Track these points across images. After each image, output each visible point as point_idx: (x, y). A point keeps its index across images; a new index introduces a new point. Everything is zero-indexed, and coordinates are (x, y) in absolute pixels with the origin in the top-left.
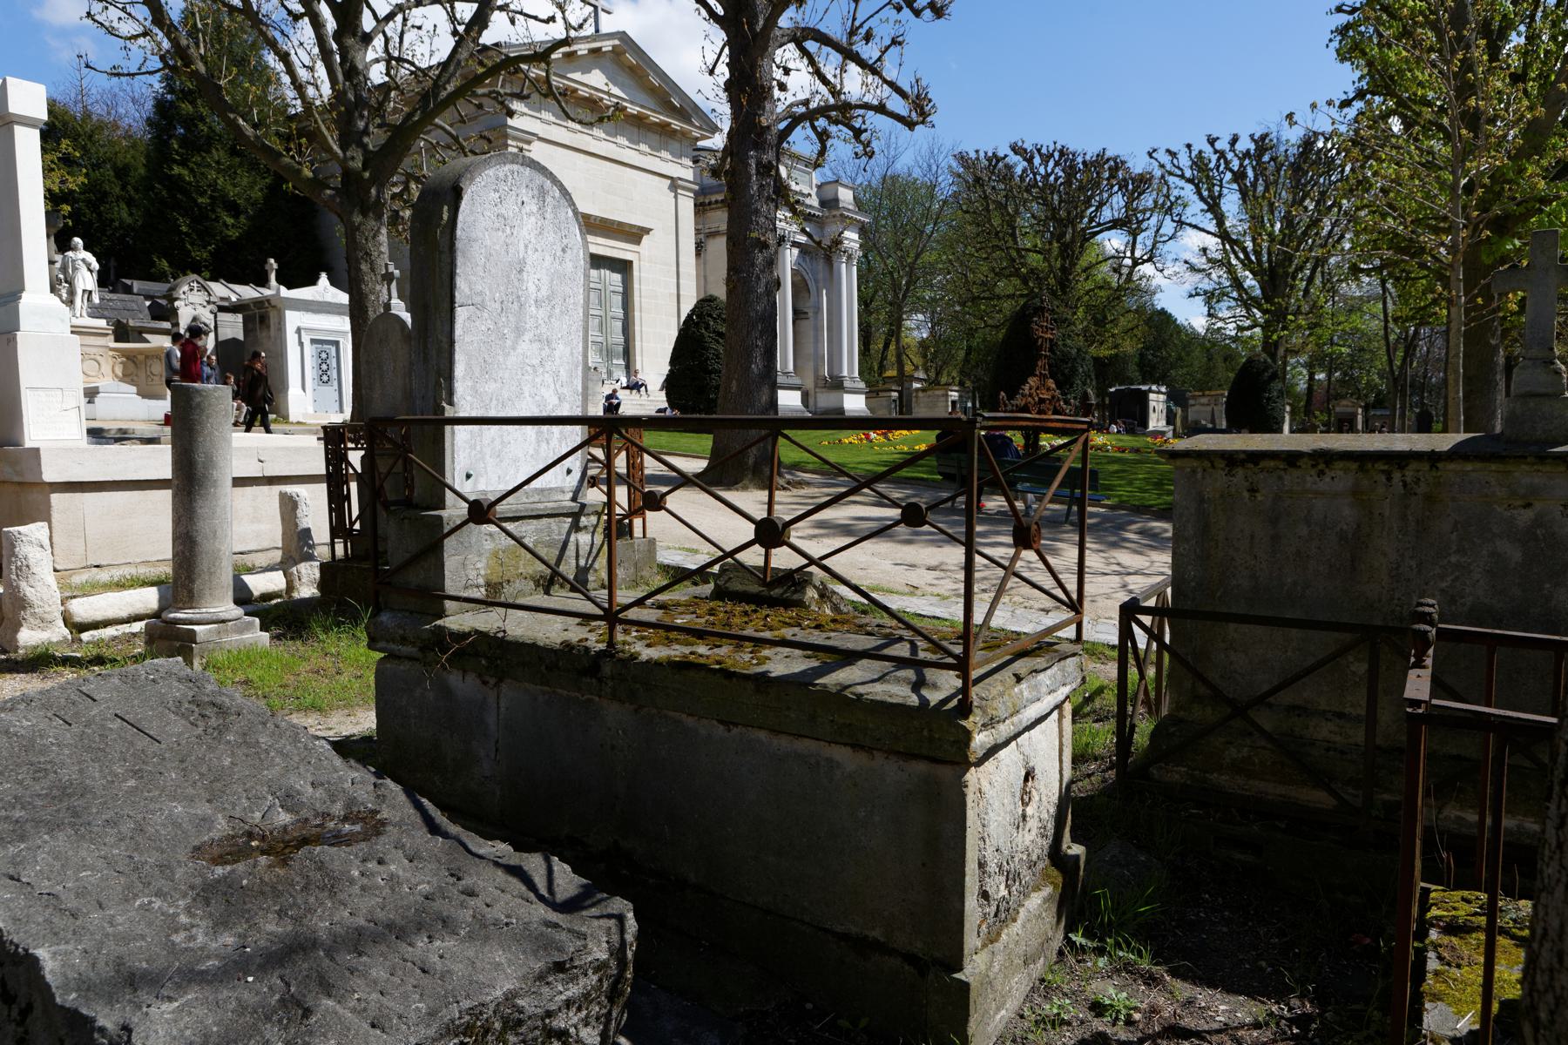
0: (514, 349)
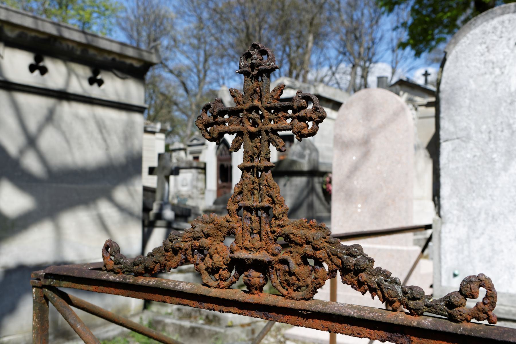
0: (505, 169)
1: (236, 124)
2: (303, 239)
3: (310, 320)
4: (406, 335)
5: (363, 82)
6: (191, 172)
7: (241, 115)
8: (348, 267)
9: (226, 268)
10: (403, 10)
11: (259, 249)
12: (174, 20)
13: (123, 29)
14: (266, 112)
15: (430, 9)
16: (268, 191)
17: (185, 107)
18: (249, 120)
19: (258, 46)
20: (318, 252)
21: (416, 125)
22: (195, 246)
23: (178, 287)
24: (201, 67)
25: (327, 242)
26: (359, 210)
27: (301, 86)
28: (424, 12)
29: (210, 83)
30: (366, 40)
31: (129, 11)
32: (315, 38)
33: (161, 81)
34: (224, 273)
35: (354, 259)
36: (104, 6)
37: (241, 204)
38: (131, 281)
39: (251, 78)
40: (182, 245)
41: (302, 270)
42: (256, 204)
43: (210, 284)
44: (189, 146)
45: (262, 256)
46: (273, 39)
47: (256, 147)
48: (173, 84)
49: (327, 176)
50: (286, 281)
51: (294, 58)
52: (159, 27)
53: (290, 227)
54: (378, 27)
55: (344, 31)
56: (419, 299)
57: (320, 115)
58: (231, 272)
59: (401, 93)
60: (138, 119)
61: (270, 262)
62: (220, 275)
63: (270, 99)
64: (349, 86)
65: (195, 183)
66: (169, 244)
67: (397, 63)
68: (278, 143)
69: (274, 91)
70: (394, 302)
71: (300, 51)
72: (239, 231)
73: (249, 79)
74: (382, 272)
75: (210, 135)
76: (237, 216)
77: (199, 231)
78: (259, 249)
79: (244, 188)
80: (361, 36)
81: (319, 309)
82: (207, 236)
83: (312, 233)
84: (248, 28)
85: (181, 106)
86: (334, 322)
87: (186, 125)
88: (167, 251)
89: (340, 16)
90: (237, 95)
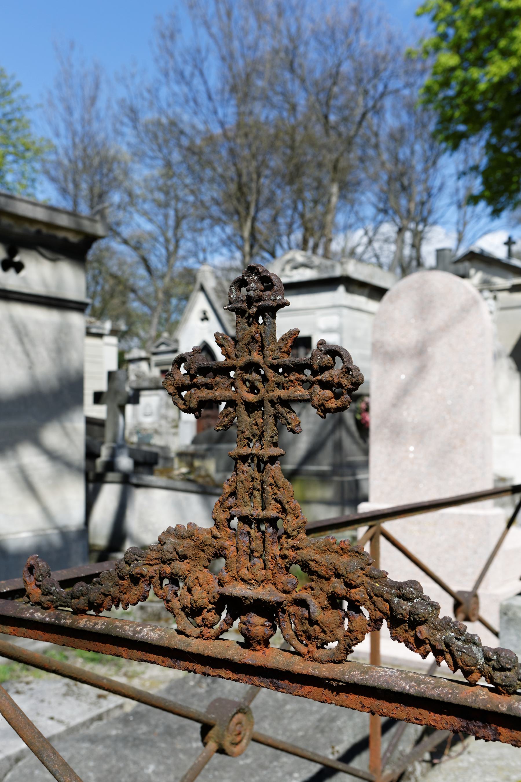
1: (225, 388)
2: (331, 569)
3: (343, 695)
4: (490, 724)
5: (414, 254)
6: (157, 395)
7: (232, 374)
8: (400, 616)
9: (213, 608)
10: (474, 145)
11: (262, 582)
12: (130, 164)
13: (53, 180)
14: (270, 373)
15: (514, 145)
16: (275, 494)
17: (148, 295)
18: (244, 383)
19: (258, 270)
20: (353, 591)
21: (494, 321)
22: (165, 573)
23: (140, 635)
24: (170, 234)
25: (367, 576)
26: (411, 456)
27: (321, 264)
28: (505, 149)
29: (185, 258)
30: (418, 189)
31: (61, 151)
32: (341, 189)
33: (111, 258)
34: (210, 616)
35: (410, 604)
36: (23, 145)
37: (234, 511)
38: (68, 621)
39: (248, 318)
40: (145, 570)
41: (328, 617)
42: (259, 512)
43: (188, 632)
44: (155, 354)
45: (266, 593)
46: (279, 192)
47: (256, 424)
48: (129, 260)
49: (363, 401)
50: (305, 632)
51: (310, 220)
52: (107, 175)
53: (309, 550)
54: (436, 170)
55: (385, 177)
56: (509, 670)
57: (354, 380)
58: (220, 615)
59: (472, 272)
60: (77, 320)
61: (279, 604)
62: (203, 619)
63: (277, 351)
64: (393, 261)
65: (163, 411)
66: (124, 568)
67: (465, 224)
68: (290, 421)
69: (282, 339)
70: (472, 672)
71: (320, 208)
72: (231, 552)
73: (244, 320)
74: (452, 625)
75: (185, 404)
76: (228, 530)
77: (171, 550)
78: (262, 582)
79: (238, 488)
80: (410, 185)
81: (356, 680)
82: (183, 558)
83: (344, 560)
84: (240, 175)
85: (140, 293)
86: (379, 699)
87: (150, 323)
88: (122, 578)
89: (379, 155)
90: (226, 344)
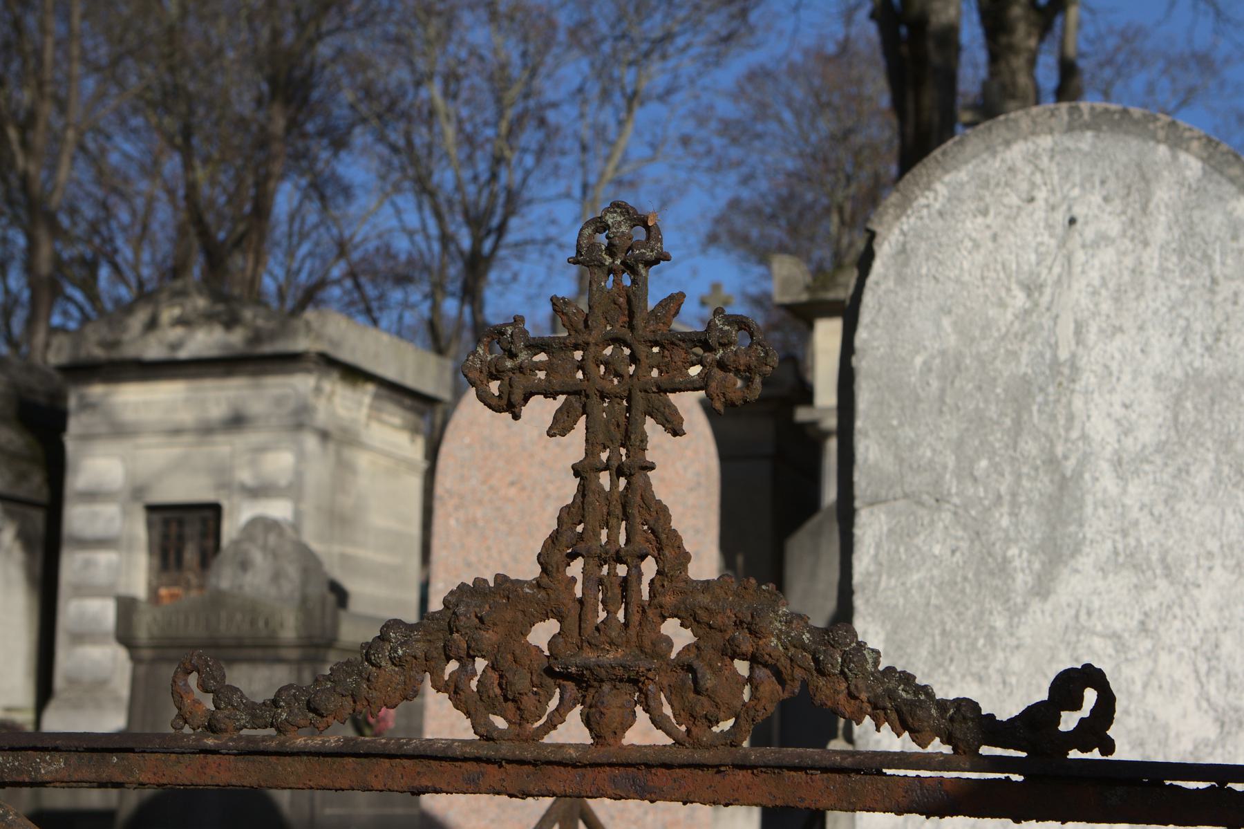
0: (1042, 589)
